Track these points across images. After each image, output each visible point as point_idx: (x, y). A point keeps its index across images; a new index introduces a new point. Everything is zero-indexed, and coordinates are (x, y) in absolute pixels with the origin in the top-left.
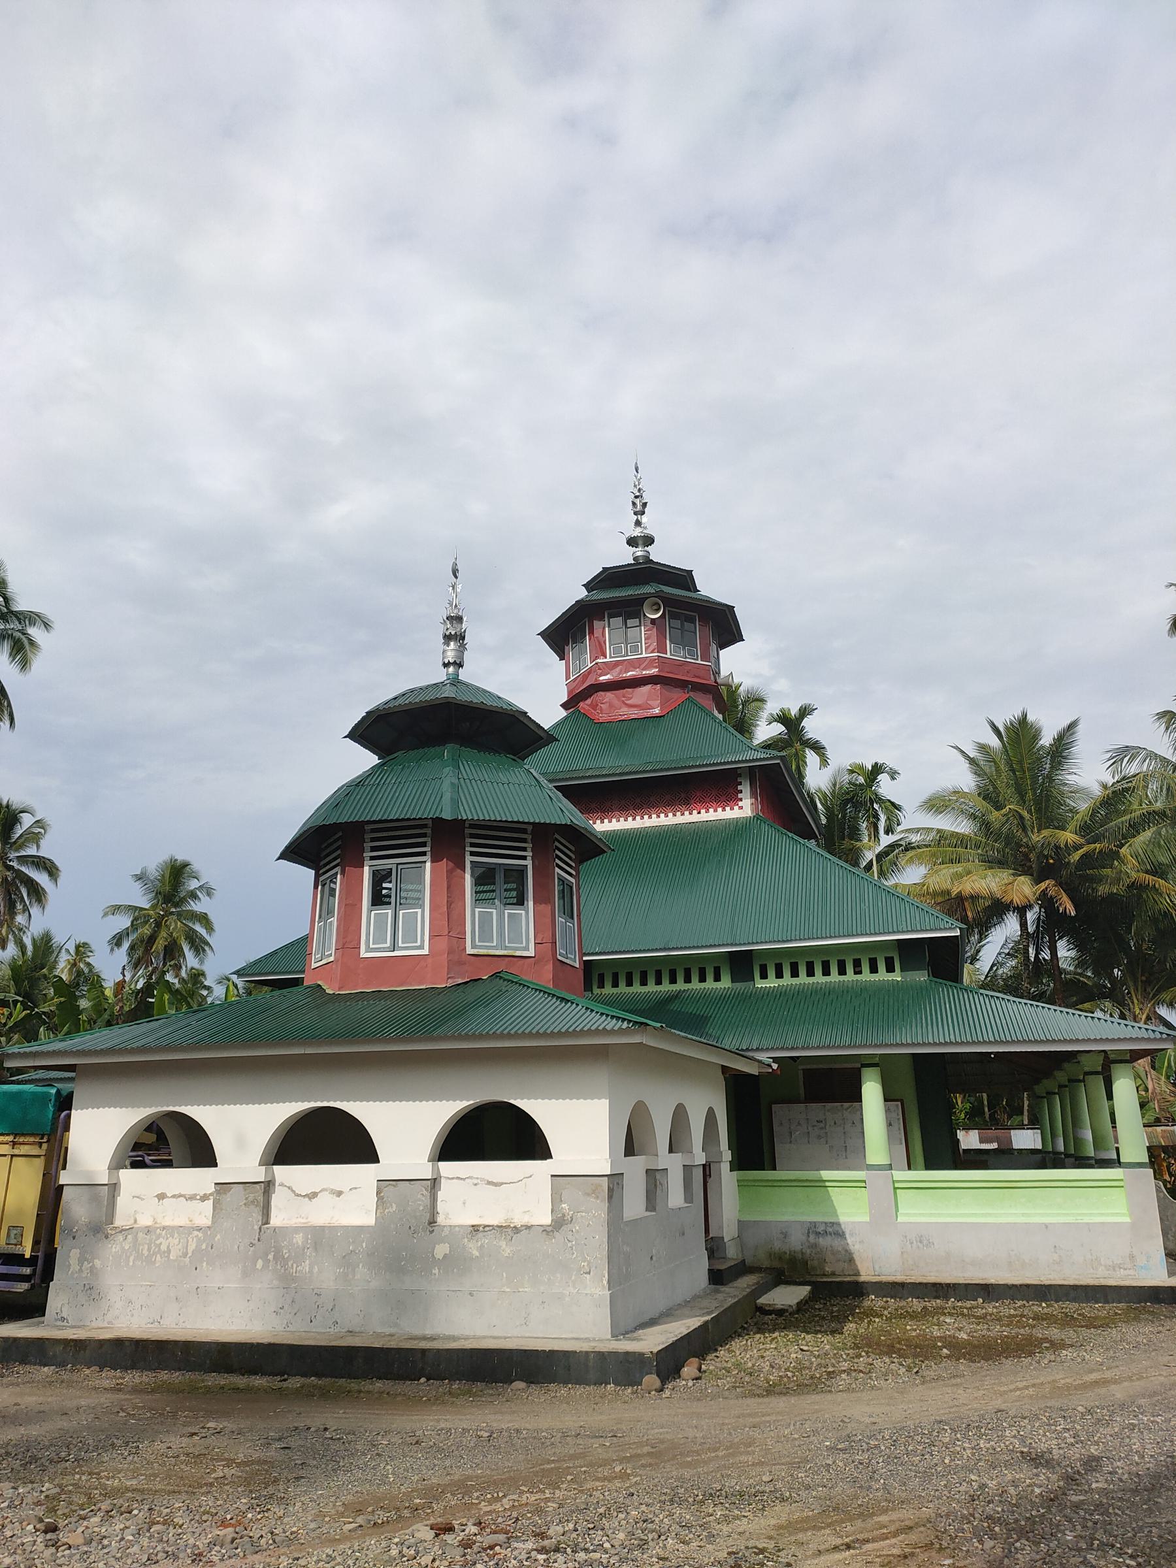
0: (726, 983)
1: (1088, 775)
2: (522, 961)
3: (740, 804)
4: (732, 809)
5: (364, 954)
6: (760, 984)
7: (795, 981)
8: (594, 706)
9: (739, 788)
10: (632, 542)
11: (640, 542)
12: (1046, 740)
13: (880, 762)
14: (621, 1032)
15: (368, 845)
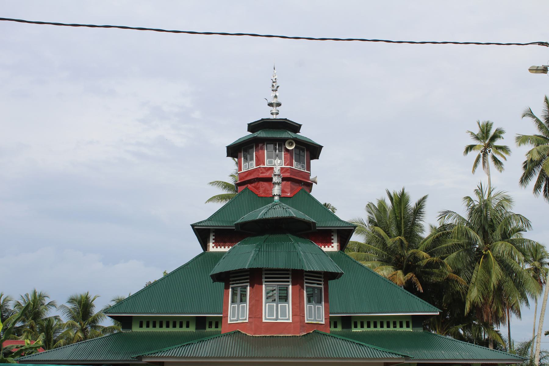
0: (339, 329)
1: (429, 224)
2: (320, 326)
3: (332, 245)
4: (328, 247)
5: (264, 321)
6: (354, 330)
7: (369, 329)
8: (258, 189)
9: (332, 237)
10: (271, 105)
11: (274, 105)
12: (412, 204)
13: (327, 203)
14: (399, 359)
15: (264, 276)
